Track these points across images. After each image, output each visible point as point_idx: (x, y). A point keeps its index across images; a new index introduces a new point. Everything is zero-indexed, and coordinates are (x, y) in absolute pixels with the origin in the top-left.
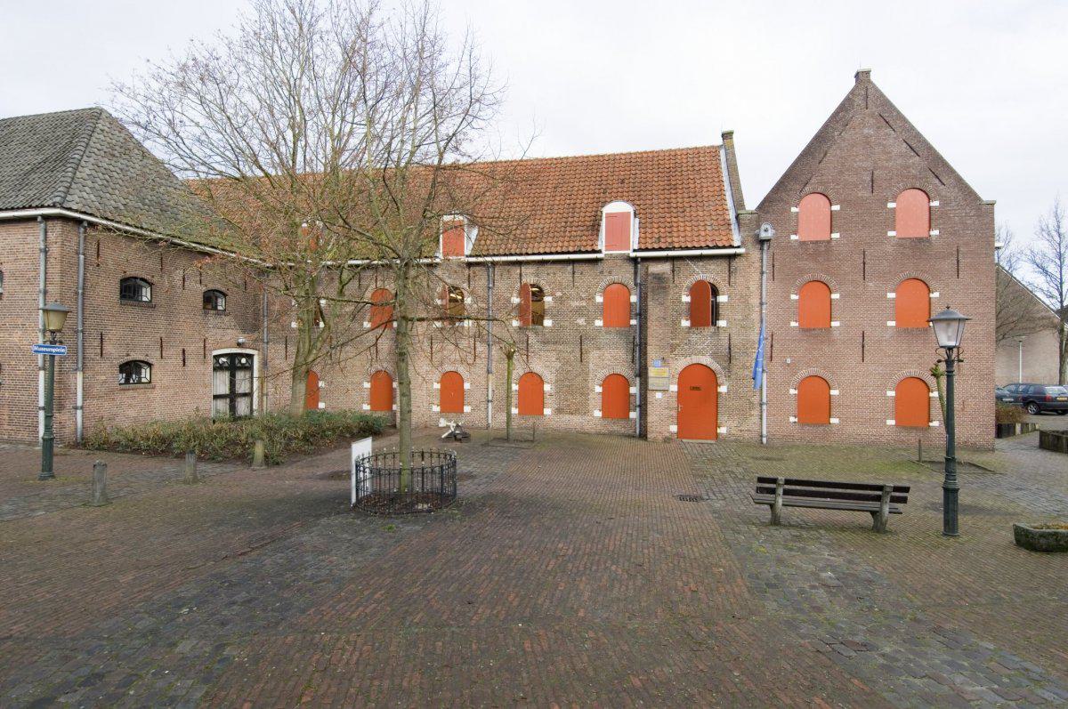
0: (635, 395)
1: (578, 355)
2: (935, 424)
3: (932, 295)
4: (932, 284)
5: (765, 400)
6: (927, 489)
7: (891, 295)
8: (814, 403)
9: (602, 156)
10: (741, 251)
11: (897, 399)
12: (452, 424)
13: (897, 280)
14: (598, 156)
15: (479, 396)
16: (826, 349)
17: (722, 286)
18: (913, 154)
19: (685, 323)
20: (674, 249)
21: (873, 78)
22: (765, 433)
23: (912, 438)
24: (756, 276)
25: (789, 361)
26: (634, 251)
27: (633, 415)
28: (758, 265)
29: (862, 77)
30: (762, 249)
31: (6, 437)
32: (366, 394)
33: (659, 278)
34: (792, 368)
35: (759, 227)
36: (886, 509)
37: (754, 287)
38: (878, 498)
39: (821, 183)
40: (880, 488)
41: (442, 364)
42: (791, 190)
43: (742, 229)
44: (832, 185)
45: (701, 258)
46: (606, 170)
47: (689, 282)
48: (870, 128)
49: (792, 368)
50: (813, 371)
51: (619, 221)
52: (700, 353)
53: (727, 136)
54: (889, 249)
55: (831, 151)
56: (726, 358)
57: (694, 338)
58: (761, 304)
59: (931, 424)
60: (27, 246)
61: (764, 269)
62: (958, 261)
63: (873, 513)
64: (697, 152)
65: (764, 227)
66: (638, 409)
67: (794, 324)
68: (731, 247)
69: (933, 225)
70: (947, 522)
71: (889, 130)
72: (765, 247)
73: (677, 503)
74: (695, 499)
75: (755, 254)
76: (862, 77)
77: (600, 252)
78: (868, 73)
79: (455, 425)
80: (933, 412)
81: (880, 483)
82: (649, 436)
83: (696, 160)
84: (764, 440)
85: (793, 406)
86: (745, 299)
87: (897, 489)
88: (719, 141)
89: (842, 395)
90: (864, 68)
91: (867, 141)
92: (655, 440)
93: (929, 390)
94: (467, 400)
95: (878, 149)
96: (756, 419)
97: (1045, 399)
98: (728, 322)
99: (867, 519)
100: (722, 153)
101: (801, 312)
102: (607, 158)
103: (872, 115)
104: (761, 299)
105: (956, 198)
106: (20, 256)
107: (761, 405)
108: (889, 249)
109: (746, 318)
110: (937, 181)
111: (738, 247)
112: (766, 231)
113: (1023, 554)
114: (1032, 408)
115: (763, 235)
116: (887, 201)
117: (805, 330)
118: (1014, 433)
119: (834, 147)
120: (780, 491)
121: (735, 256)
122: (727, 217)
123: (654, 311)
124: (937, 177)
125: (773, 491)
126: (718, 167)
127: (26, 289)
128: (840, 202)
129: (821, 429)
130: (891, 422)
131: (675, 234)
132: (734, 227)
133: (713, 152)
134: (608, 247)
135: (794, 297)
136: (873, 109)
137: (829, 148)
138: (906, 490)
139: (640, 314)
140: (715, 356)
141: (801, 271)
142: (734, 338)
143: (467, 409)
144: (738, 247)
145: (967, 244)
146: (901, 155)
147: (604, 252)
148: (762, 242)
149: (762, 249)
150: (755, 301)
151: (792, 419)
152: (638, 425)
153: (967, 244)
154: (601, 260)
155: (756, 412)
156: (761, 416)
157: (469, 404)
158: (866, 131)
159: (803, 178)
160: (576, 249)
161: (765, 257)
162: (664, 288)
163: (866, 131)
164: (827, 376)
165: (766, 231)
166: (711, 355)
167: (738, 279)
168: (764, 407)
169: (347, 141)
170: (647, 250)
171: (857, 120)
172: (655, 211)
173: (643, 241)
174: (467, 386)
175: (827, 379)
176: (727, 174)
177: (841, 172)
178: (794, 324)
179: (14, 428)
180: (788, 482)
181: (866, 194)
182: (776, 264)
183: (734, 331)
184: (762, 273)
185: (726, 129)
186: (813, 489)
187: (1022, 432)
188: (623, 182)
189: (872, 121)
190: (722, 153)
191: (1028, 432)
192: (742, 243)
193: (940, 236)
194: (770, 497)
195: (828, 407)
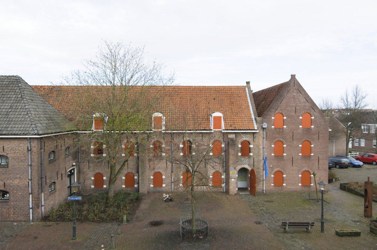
0: (223, 179)
1: (204, 165)
2: (312, 184)
3: (311, 146)
4: (312, 142)
5: (264, 179)
6: (318, 225)
7: (300, 146)
8: (279, 178)
9: (205, 87)
10: (257, 131)
11: (302, 177)
12: (168, 196)
13: (302, 141)
14: (204, 87)
15: (169, 181)
16: (282, 162)
17: (251, 142)
18: (307, 102)
19: (240, 154)
20: (236, 130)
21: (296, 77)
22: (264, 189)
23: (306, 189)
24: (262, 139)
25: (271, 166)
26: (223, 130)
27: (223, 185)
28: (262, 135)
29: (293, 77)
30: (263, 130)
31: (12, 219)
32: (123, 181)
33: (232, 140)
34: (272, 169)
35: (262, 123)
36: (310, 228)
37: (261, 142)
38: (308, 225)
39: (281, 110)
40: (309, 223)
41: (154, 169)
42: (272, 111)
43: (257, 123)
44: (284, 111)
45: (245, 133)
46: (208, 93)
47: (240, 141)
48: (295, 93)
49: (272, 169)
50: (278, 169)
51: (217, 119)
52: (245, 164)
53: (248, 83)
54: (300, 131)
55: (284, 100)
56: (253, 166)
57: (243, 159)
58: (263, 148)
59: (311, 185)
60: (20, 148)
61: (264, 137)
62: (319, 136)
63: (306, 228)
64: (238, 88)
65: (264, 124)
66: (225, 183)
67: (273, 154)
68: (254, 130)
69: (312, 124)
70: (322, 229)
71: (300, 94)
72: (264, 130)
73: (255, 224)
74: (260, 223)
75: (261, 132)
76: (293, 77)
77: (211, 130)
78: (295, 75)
79: (168, 196)
80: (312, 181)
81: (308, 222)
82: (230, 193)
83: (238, 92)
84: (264, 192)
85: (272, 181)
86: (258, 146)
87: (312, 223)
88: (245, 84)
89: (287, 177)
90: (293, 74)
91: (294, 97)
92: (232, 195)
93: (311, 174)
94: (164, 182)
95: (297, 100)
96: (261, 185)
97: (341, 163)
98: (253, 154)
99: (305, 229)
100: (247, 89)
101: (275, 151)
102: (207, 88)
103: (296, 89)
104: (263, 146)
105: (319, 116)
106: (17, 151)
107: (263, 180)
108: (300, 131)
109: (259, 152)
110: (313, 111)
111: (256, 130)
112: (265, 125)
113: (337, 237)
114: (338, 166)
115: (264, 127)
116: (299, 116)
117: (276, 156)
118: (333, 182)
119: (285, 99)
120: (287, 225)
121: (255, 133)
122: (252, 118)
123: (231, 151)
124: (314, 110)
125: (285, 225)
126: (246, 96)
127: (21, 164)
128: (286, 116)
129: (280, 187)
130: (300, 184)
131: (236, 124)
132: (254, 121)
133: (243, 88)
134: (214, 128)
135: (273, 146)
136: (296, 87)
137: (283, 99)
138: (314, 223)
139: (225, 151)
140: (249, 165)
141: (275, 138)
142: (255, 159)
143: (164, 185)
144: (256, 130)
145: (321, 131)
146: (304, 102)
147: (213, 130)
148: (264, 128)
149: (263, 130)
150: (261, 147)
151: (272, 185)
152: (225, 189)
153: (321, 131)
154: (211, 133)
155: (261, 183)
156: (263, 184)
157: (164, 184)
158: (294, 94)
159: (276, 108)
160: (203, 129)
161: (264, 133)
162: (235, 144)
163: (294, 94)
164: (283, 171)
165: (265, 125)
166: (248, 165)
167: (256, 140)
168: (264, 181)
169: (114, 83)
170: (227, 130)
171: (291, 91)
172: (228, 113)
173: (226, 126)
174: (164, 177)
175: (282, 172)
176: (250, 100)
177: (286, 107)
178: (273, 154)
179: (16, 216)
180: (289, 223)
181: (293, 114)
182: (268, 135)
183: (255, 156)
184: (263, 138)
185: (248, 81)
186: (294, 224)
187: (335, 181)
188: (214, 99)
189: (296, 91)
190: (247, 89)
191: (337, 181)
192: (257, 128)
193: (314, 128)
194: (284, 227)
195: (283, 180)
